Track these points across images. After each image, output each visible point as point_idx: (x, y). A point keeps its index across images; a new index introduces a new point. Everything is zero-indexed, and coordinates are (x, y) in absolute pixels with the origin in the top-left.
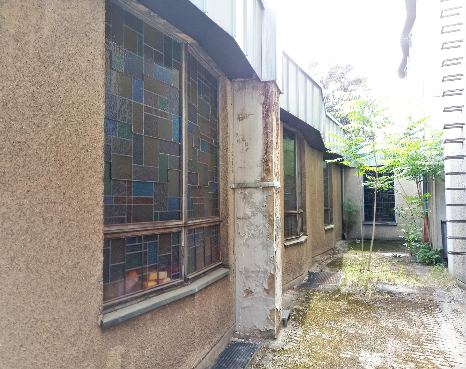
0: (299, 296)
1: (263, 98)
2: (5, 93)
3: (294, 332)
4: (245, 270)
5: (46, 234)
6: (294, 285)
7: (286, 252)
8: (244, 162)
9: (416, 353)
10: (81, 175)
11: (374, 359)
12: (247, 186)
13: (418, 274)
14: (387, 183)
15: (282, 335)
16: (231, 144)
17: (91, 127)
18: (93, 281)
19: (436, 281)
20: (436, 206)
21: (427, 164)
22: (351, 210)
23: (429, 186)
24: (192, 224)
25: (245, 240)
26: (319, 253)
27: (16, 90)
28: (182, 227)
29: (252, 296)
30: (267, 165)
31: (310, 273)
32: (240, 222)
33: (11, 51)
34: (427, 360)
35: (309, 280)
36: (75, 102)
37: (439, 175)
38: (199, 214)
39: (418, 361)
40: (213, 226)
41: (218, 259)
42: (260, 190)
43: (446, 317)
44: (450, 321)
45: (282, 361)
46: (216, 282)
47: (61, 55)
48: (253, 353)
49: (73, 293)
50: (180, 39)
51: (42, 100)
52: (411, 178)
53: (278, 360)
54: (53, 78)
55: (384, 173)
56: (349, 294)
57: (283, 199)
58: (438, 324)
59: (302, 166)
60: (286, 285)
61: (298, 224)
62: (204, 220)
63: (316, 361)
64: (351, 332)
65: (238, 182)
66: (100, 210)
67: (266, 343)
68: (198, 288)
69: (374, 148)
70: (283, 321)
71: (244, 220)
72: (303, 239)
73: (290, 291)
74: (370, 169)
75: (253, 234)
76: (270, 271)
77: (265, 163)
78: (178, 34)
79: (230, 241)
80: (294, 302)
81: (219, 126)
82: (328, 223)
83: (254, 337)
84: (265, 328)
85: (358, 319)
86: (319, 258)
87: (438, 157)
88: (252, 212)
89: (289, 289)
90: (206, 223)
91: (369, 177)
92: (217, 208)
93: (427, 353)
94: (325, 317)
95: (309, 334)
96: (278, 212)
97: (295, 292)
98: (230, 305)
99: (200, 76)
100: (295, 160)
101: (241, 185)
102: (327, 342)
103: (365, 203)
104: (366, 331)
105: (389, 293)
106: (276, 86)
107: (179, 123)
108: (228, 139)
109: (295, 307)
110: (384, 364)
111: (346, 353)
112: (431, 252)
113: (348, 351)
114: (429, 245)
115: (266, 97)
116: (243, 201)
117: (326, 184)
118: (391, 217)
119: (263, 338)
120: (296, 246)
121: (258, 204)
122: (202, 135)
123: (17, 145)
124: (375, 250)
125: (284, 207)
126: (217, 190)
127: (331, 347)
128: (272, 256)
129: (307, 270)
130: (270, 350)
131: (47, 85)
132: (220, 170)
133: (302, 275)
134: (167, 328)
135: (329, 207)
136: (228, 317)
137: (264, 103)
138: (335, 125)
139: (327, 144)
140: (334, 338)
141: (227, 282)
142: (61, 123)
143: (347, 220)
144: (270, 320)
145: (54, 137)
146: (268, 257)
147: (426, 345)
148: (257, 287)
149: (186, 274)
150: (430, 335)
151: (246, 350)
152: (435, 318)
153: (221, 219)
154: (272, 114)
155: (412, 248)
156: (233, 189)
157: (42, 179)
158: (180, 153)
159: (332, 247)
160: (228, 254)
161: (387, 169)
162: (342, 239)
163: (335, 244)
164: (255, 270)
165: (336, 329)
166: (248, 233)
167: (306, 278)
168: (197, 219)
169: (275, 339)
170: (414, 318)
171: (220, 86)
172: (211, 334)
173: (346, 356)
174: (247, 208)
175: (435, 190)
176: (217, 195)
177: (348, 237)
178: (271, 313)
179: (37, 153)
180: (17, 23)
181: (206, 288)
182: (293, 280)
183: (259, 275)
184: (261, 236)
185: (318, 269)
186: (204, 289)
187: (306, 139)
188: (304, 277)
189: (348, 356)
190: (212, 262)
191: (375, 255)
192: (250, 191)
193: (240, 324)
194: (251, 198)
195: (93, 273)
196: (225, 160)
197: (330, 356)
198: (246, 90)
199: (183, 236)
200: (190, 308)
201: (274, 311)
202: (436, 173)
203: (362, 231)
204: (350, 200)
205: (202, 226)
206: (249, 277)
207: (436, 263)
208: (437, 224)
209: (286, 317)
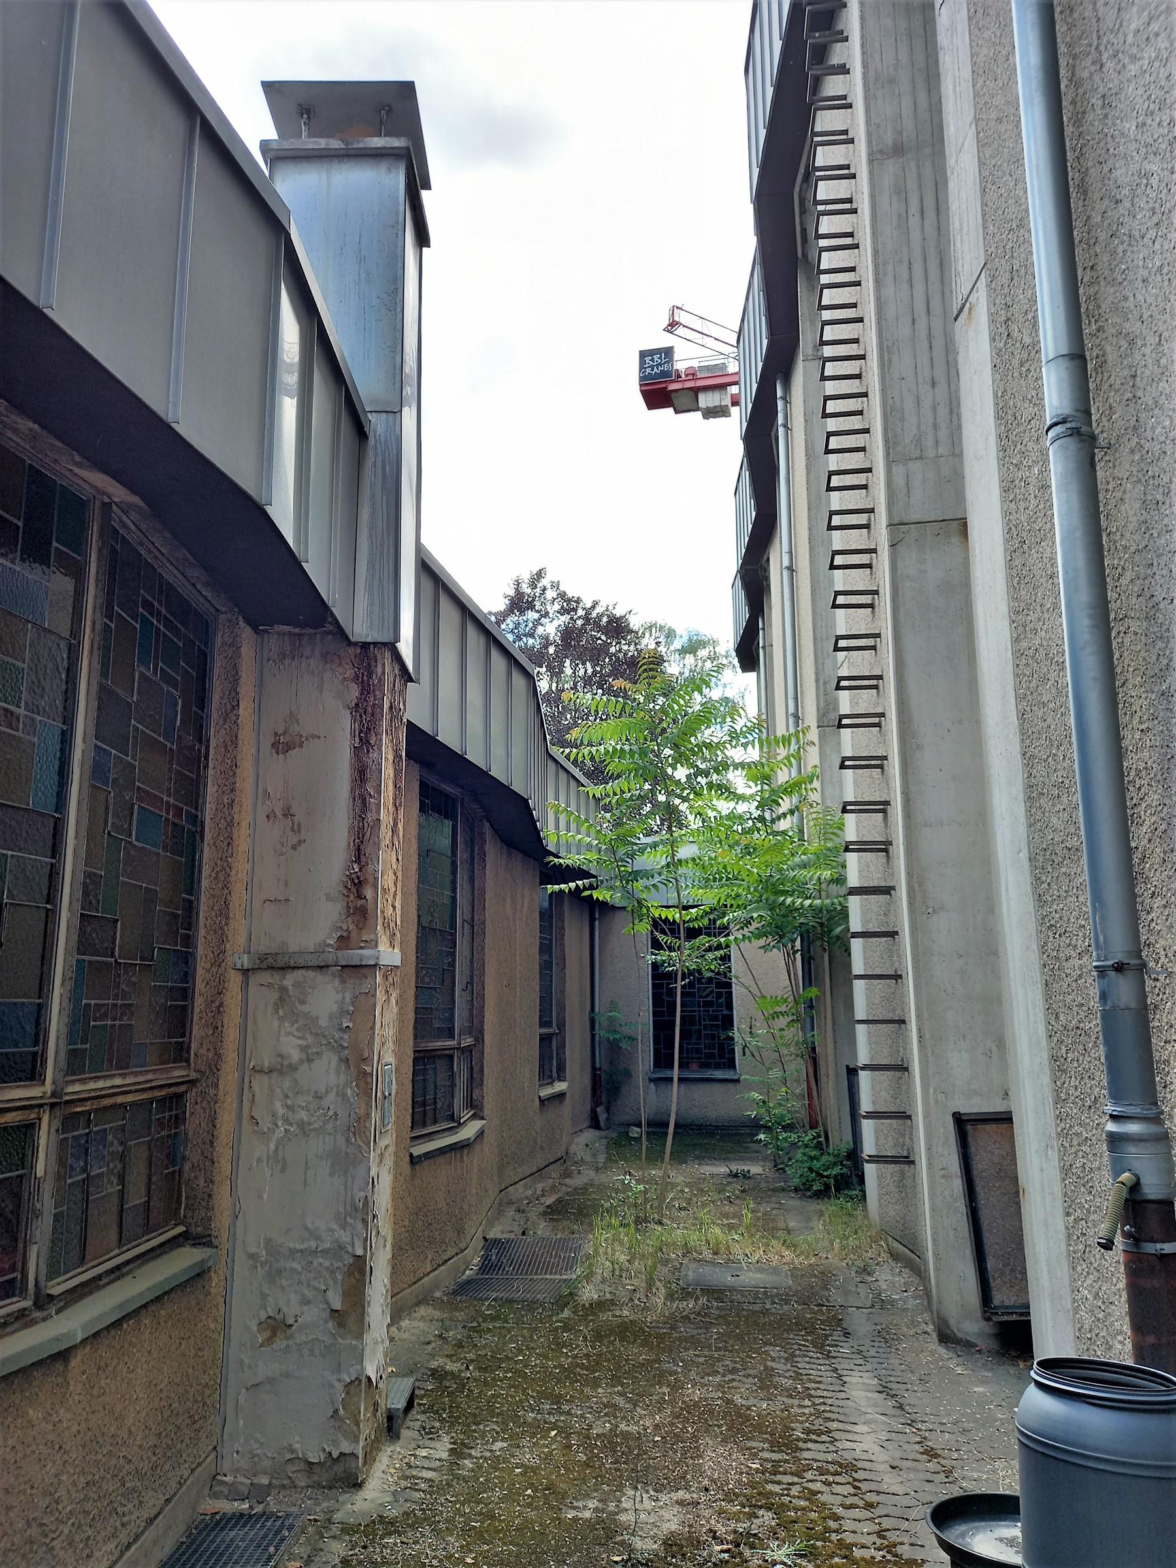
0: (447, 1323)
1: (354, 691)
3: (424, 1453)
4: (266, 1248)
6: (436, 1287)
7: (413, 1176)
8: (286, 884)
9: (779, 1477)
11: (662, 1512)
12: (292, 964)
13: (792, 1224)
14: (710, 955)
15: (384, 1467)
16: (244, 824)
19: (836, 1245)
20: (834, 1024)
21: (808, 902)
22: (617, 1037)
23: (816, 968)
24: (82, 1096)
25: (272, 1146)
26: (521, 1176)
28: (41, 1106)
29: (288, 1338)
30: (360, 896)
31: (490, 1244)
32: (260, 1085)
34: (808, 1495)
35: (485, 1267)
37: (838, 937)
38: (110, 1061)
39: (783, 1504)
40: (161, 1101)
41: (172, 1216)
42: (334, 976)
43: (860, 1352)
44: (869, 1367)
46: (158, 1299)
48: (277, 1550)
50: (87, 487)
52: (772, 944)
55: (706, 928)
56: (600, 1305)
57: (411, 1005)
59: (477, 901)
60: (408, 1291)
61: (457, 1082)
62: (128, 1081)
63: (486, 1547)
64: (600, 1431)
65: (263, 949)
67: (325, 1504)
68: (84, 1327)
69: (673, 855)
70: (390, 1417)
71: (274, 1075)
72: (469, 1131)
73: (422, 1311)
74: (664, 913)
75: (303, 1122)
76: (353, 1246)
77: (354, 890)
78: (76, 470)
79: (218, 1148)
80: (429, 1348)
81: (206, 766)
82: (551, 1077)
83: (284, 1487)
84: (324, 1450)
85: (622, 1385)
86: (521, 1190)
87: (833, 887)
88: (303, 1049)
89: (419, 1303)
90: (137, 1091)
91: (661, 937)
92: (183, 1035)
93: (809, 1475)
94: (524, 1390)
95: (470, 1456)
96: (390, 1045)
97: (437, 1314)
98: (205, 1379)
99: (147, 605)
100: (454, 882)
101: (270, 960)
102: (523, 1474)
103: (655, 1014)
105: (714, 1291)
106: (398, 658)
107: (62, 750)
108: (236, 809)
109: (434, 1364)
110: (691, 1526)
111: (580, 1504)
112: (824, 1159)
113: (587, 1496)
114: (819, 1136)
115: (363, 689)
116: (277, 1011)
117: (546, 957)
119: (318, 1486)
120: (448, 1155)
121: (324, 1022)
122: (143, 790)
124: (679, 1157)
125: (415, 1028)
126: (188, 976)
127: (535, 1490)
128: (362, 1194)
129: (479, 1235)
130: (335, 1530)
132: (203, 908)
133: (462, 1251)
135: (554, 1025)
136: (197, 1426)
137: (357, 705)
138: (573, 783)
140: (548, 1457)
141: (202, 1297)
143: (605, 1067)
146: (349, 1199)
147: (808, 1449)
148: (305, 1308)
149: (42, 1278)
150: (818, 1414)
151: (252, 1541)
152: (833, 1361)
153: (193, 1075)
154: (381, 740)
155: (778, 1148)
156: (245, 972)
158: (56, 847)
159: (559, 1155)
161: (711, 917)
162: (591, 1127)
163: (571, 1143)
164: (303, 1247)
165: (554, 1426)
166: (286, 1120)
167: (476, 1260)
168: (105, 1077)
169: (358, 1486)
170: (778, 1366)
171: (219, 640)
172: (123, 1495)
173: (580, 1515)
174: (289, 1034)
175: (831, 980)
176: (186, 993)
177: (608, 1119)
178: (347, 1393)
181: (117, 1324)
182: (434, 1270)
183: (315, 1264)
184: (329, 1127)
185: (516, 1229)
186: (107, 1328)
187: (488, 821)
188: (469, 1259)
189: (587, 1514)
190: (149, 1228)
191: (680, 1175)
192: (301, 979)
193: (236, 1446)
194: (303, 1002)
196: (221, 877)
197: (532, 1522)
198: (304, 664)
199: (43, 1142)
200: (48, 1406)
202: (830, 931)
204: (613, 1006)
205: (120, 1100)
206: (279, 1272)
207: (838, 1189)
208: (837, 1076)
209: (401, 1404)
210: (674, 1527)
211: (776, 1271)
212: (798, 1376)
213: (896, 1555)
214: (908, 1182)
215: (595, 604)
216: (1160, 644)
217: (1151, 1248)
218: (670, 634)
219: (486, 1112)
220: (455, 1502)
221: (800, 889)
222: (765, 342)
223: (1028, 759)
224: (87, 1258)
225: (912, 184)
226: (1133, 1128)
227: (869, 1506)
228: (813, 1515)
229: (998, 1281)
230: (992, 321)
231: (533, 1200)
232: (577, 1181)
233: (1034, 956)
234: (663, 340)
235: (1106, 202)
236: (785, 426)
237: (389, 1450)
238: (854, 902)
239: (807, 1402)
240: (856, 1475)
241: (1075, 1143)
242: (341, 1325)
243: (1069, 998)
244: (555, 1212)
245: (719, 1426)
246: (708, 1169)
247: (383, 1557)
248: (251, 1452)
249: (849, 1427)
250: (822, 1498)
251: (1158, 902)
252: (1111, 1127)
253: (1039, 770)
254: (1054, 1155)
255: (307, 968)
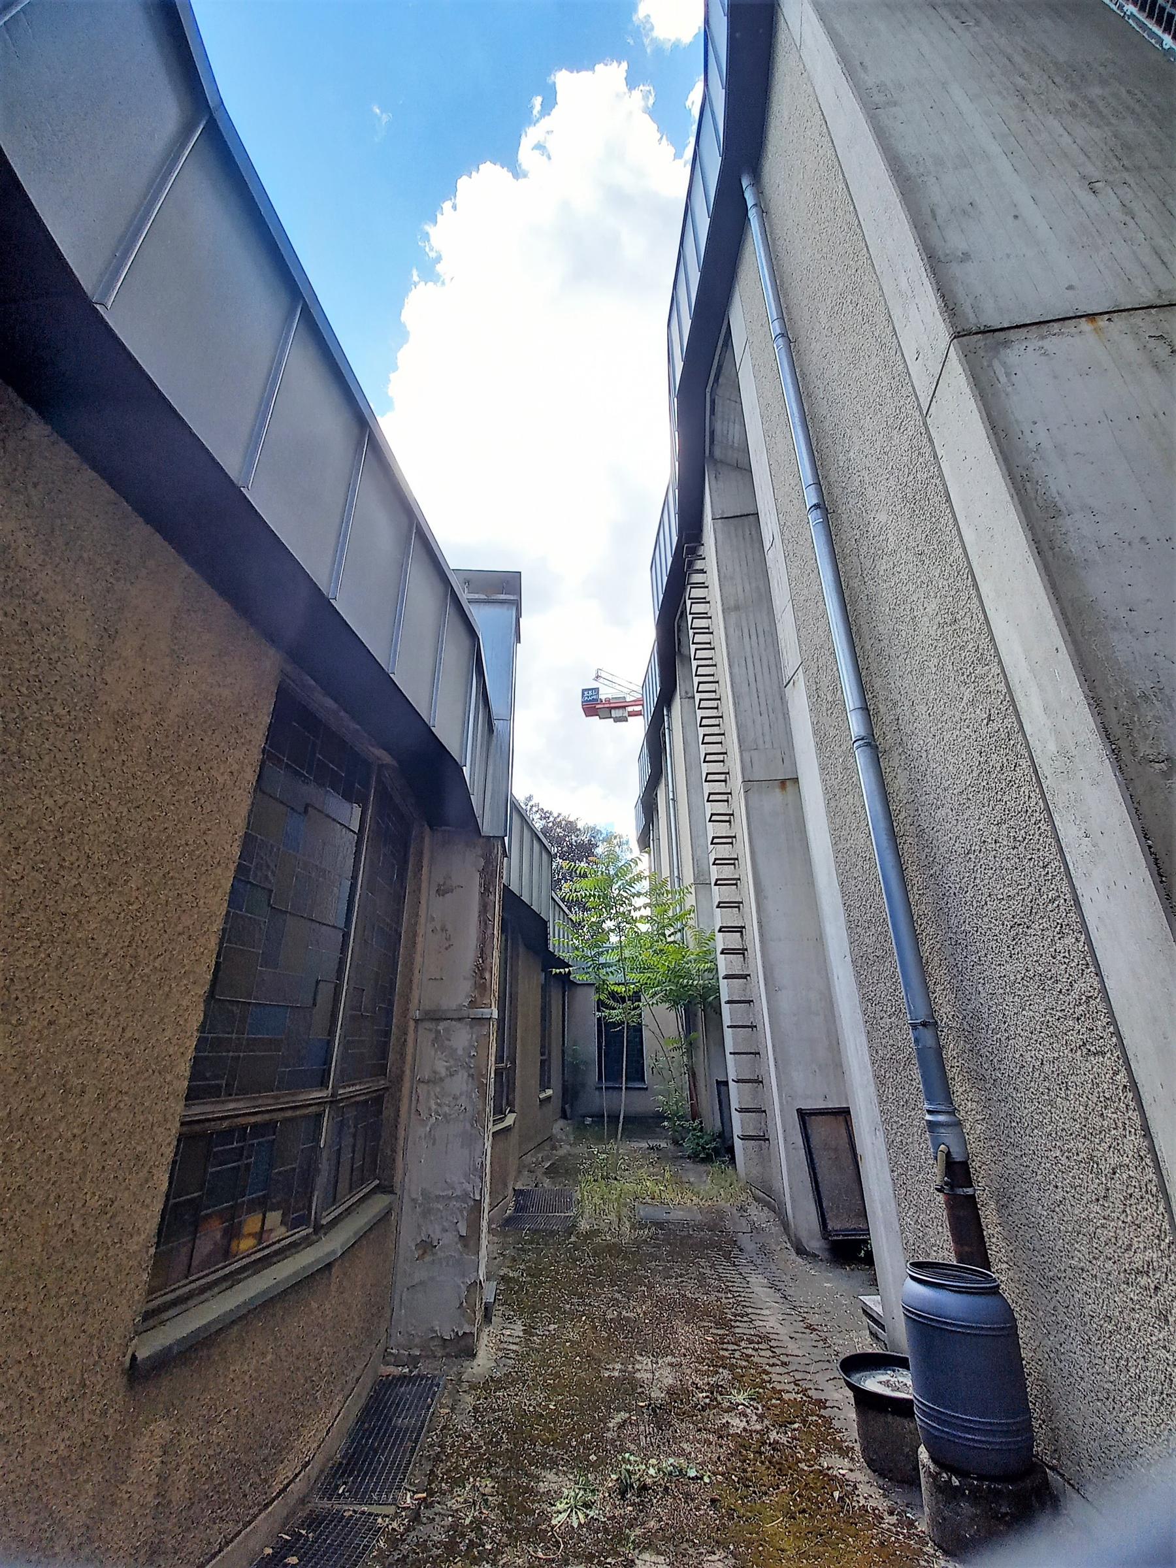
2: (65, 814)
5: (62, 1127)
9: (725, 1346)
10: (167, 989)
13: (692, 1180)
17: (207, 891)
18: (135, 1247)
25: (428, 1129)
27: (89, 810)
29: (434, 1254)
32: (422, 1089)
33: (102, 739)
35: (519, 1208)
36: (191, 842)
45: (494, 1411)
47: (187, 758)
48: (432, 1401)
49: (84, 1283)
51: (131, 834)
53: (485, 1410)
54: (162, 796)
56: (593, 1233)
58: (744, 1278)
63: (560, 1398)
65: (427, 1008)
66: (184, 1068)
74: (616, 988)
78: (370, 748)
93: (743, 1344)
104: (636, 1311)
111: (610, 1366)
118: (637, 1073)
119: (448, 1356)
123: (57, 918)
126: (389, 1024)
127: (582, 1359)
130: (465, 1386)
131: (149, 806)
134: (269, 1357)
139: (553, 943)
142: (156, 880)
144: (464, 1309)
145: (135, 907)
148: (444, 1235)
156: (416, 1021)
157: (87, 995)
160: (394, 1160)
162: (561, 1117)
176: (387, 1034)
179: (93, 939)
180: (126, 695)
183: (451, 1205)
195: (139, 1224)
201: (476, 1285)
203: (604, 1101)
210: (671, 1382)
211: (690, 1210)
212: (720, 1279)
213: (809, 1397)
214: (765, 1152)
215: (559, 815)
216: (927, 850)
217: (960, 1191)
218: (599, 832)
219: (516, 1109)
220: (535, 1366)
221: (688, 975)
222: (659, 689)
223: (847, 907)
224: (338, 1197)
225: (744, 624)
226: (941, 1118)
227: (784, 1364)
228: (753, 1371)
229: (830, 1214)
230: (808, 688)
231: (537, 1164)
232: (562, 1152)
233: (859, 1016)
234: (594, 685)
235: (873, 641)
236: (669, 728)
237: (487, 1330)
238: (723, 983)
239: (729, 1295)
240: (771, 1344)
241: (894, 1127)
242: (465, 1246)
243: (884, 1041)
244: (552, 1172)
245: (682, 1312)
246: (635, 1145)
247: (498, 1406)
248: (407, 1332)
249: (758, 1311)
250: (755, 1359)
251: (939, 987)
252: (928, 1117)
253: (856, 914)
254: (880, 1134)
255: (452, 1019)
